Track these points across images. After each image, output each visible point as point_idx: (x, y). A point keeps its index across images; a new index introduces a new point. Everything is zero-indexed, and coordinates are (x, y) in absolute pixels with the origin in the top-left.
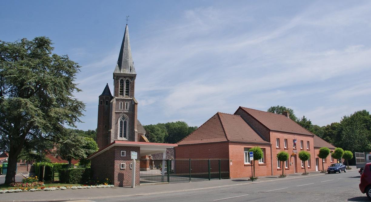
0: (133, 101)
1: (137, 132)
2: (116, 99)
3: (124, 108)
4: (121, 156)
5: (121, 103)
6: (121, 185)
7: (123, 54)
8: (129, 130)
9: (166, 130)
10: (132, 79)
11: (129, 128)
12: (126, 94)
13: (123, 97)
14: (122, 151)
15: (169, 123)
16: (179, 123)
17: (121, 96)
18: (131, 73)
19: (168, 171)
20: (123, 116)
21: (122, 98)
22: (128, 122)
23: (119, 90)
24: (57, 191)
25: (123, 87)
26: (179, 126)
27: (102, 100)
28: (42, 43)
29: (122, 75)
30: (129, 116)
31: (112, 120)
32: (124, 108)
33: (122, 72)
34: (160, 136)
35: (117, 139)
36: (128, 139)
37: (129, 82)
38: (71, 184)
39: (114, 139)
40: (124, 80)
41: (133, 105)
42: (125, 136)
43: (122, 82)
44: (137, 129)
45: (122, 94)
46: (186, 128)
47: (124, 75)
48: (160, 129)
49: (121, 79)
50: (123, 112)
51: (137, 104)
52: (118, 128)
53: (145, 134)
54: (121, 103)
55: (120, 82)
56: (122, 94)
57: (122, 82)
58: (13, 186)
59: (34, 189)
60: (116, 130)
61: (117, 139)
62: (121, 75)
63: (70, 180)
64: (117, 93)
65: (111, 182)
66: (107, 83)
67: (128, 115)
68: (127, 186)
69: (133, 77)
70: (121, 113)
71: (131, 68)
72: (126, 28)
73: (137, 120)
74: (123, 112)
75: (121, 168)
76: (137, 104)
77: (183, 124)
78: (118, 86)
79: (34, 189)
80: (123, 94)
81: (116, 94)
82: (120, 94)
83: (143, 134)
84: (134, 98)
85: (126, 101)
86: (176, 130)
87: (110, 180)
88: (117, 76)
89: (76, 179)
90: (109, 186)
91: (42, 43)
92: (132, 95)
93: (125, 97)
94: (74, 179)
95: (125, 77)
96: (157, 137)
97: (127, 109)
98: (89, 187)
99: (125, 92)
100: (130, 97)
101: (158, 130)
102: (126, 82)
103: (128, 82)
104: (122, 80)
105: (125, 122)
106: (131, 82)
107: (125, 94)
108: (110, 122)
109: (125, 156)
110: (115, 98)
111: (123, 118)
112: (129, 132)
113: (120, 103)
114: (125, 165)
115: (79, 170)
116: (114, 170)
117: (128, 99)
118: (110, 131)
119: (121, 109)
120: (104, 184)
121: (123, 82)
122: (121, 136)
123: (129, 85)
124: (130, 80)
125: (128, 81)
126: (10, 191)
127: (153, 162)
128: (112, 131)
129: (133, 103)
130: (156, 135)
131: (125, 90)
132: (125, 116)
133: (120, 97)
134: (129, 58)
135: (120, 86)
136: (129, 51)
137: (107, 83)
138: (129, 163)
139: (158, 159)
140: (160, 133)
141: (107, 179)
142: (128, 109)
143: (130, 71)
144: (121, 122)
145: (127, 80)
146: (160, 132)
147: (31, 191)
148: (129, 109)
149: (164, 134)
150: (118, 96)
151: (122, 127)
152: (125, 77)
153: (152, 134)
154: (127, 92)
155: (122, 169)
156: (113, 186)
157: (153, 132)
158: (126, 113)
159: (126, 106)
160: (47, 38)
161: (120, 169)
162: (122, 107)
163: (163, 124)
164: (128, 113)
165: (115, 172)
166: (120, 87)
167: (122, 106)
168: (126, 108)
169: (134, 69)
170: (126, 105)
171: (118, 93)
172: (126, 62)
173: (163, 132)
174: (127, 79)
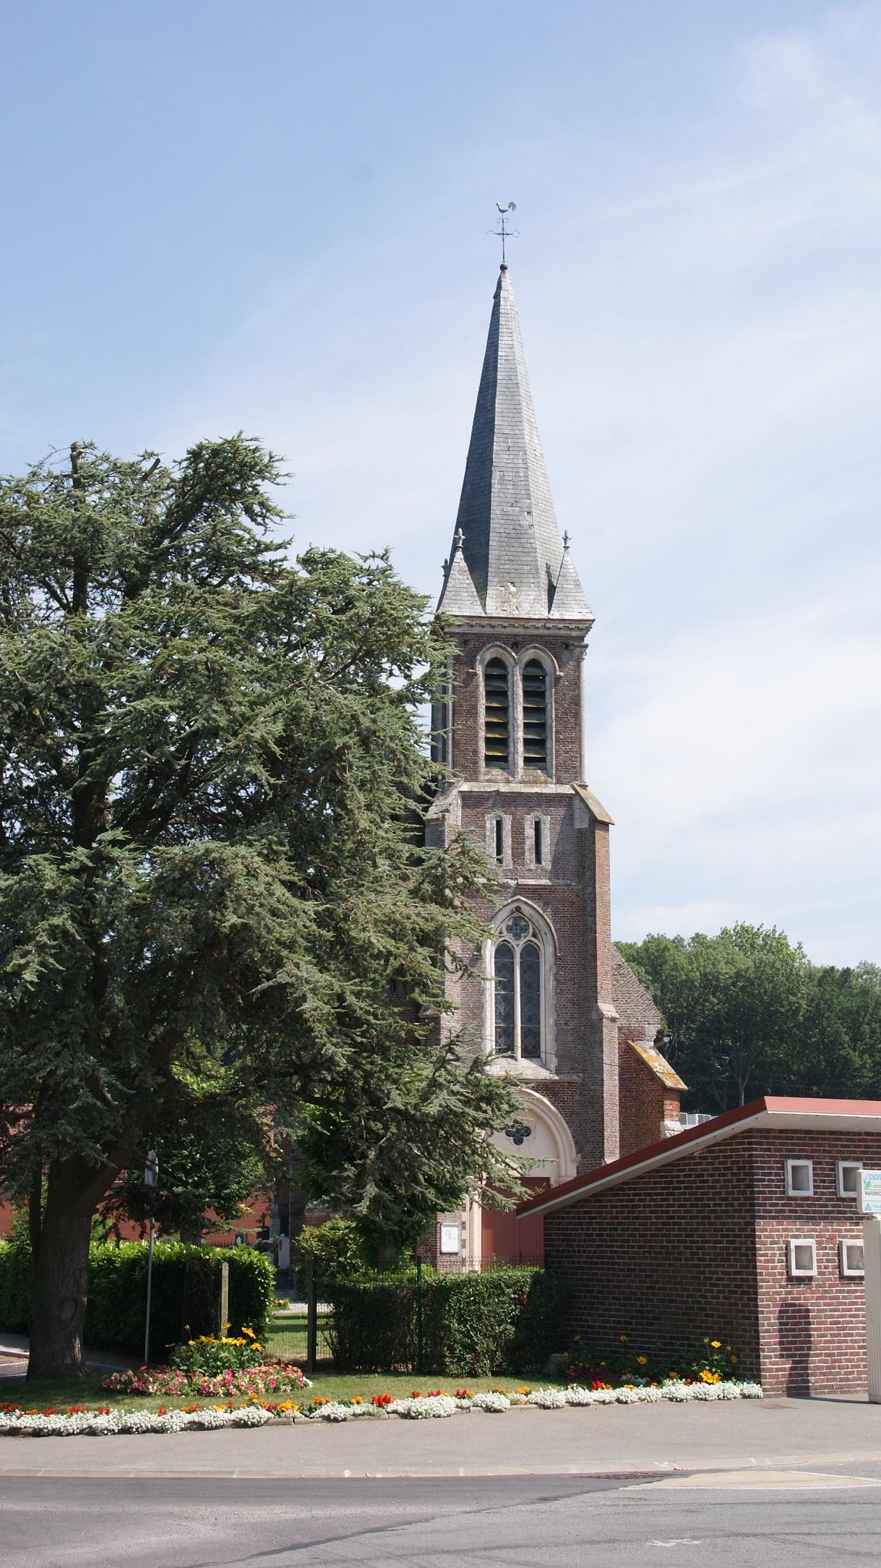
0: (577, 803)
1: (613, 1020)
2: (465, 796)
3: (518, 854)
4: (791, 1193)
5: (499, 824)
6: (798, 1388)
7: (495, 481)
8: (558, 1009)
10: (565, 654)
11: (559, 992)
12: (527, 760)
13: (508, 782)
14: (791, 1163)
16: (744, 938)
17: (496, 773)
18: (555, 615)
20: (518, 909)
21: (504, 788)
22: (550, 949)
23: (482, 734)
24: (466, 1417)
26: (745, 962)
28: (224, 476)
30: (555, 913)
32: (518, 854)
33: (494, 608)
36: (553, 1067)
38: (457, 1376)
40: (509, 662)
41: (583, 836)
42: (531, 1052)
43: (497, 672)
45: (500, 760)
46: (792, 976)
49: (489, 655)
50: (512, 883)
51: (605, 825)
53: (652, 1030)
54: (499, 824)
57: (497, 672)
58: (144, 1393)
59: (341, 1411)
62: (488, 630)
63: (452, 1349)
65: (741, 1366)
67: (546, 905)
68: (832, 1390)
69: (567, 642)
71: (549, 574)
72: (497, 296)
74: (512, 883)
75: (796, 1272)
76: (605, 825)
77: (775, 944)
78: (475, 707)
79: (341, 1411)
80: (504, 759)
82: (488, 758)
83: (640, 1035)
84: (584, 787)
85: (531, 810)
86: (715, 990)
87: (732, 1353)
89: (483, 1344)
90: (733, 1388)
91: (224, 476)
92: (572, 768)
93: (521, 780)
94: (470, 1348)
95: (516, 644)
97: (538, 860)
98: (583, 1394)
99: (521, 747)
100: (559, 782)
102: (526, 678)
104: (496, 663)
105: (531, 953)
106: (558, 679)
107: (521, 762)
109: (810, 1193)
110: (455, 792)
111: (518, 924)
112: (557, 1023)
113: (490, 824)
114: (814, 1252)
115: (496, 1287)
116: (756, 1287)
117: (545, 790)
120: (701, 1380)
121: (504, 678)
122: (505, 1047)
123: (542, 695)
124: (548, 661)
125: (533, 671)
126: (102, 1421)
131: (520, 734)
132: (525, 909)
133: (492, 781)
135: (482, 703)
136: (530, 456)
138: (832, 1238)
141: (716, 1344)
142: (547, 863)
143: (544, 597)
144: (503, 952)
145: (534, 663)
147: (327, 1419)
148: (555, 861)
151: (513, 990)
152: (516, 644)
154: (536, 744)
155: (800, 1280)
156: (753, 1388)
158: (534, 892)
159: (530, 843)
160: (253, 445)
161: (790, 1279)
164: (544, 887)
165: (762, 1301)
166: (488, 708)
168: (530, 855)
169: (578, 585)
170: (530, 832)
171: (476, 752)
172: (519, 535)
174: (529, 654)
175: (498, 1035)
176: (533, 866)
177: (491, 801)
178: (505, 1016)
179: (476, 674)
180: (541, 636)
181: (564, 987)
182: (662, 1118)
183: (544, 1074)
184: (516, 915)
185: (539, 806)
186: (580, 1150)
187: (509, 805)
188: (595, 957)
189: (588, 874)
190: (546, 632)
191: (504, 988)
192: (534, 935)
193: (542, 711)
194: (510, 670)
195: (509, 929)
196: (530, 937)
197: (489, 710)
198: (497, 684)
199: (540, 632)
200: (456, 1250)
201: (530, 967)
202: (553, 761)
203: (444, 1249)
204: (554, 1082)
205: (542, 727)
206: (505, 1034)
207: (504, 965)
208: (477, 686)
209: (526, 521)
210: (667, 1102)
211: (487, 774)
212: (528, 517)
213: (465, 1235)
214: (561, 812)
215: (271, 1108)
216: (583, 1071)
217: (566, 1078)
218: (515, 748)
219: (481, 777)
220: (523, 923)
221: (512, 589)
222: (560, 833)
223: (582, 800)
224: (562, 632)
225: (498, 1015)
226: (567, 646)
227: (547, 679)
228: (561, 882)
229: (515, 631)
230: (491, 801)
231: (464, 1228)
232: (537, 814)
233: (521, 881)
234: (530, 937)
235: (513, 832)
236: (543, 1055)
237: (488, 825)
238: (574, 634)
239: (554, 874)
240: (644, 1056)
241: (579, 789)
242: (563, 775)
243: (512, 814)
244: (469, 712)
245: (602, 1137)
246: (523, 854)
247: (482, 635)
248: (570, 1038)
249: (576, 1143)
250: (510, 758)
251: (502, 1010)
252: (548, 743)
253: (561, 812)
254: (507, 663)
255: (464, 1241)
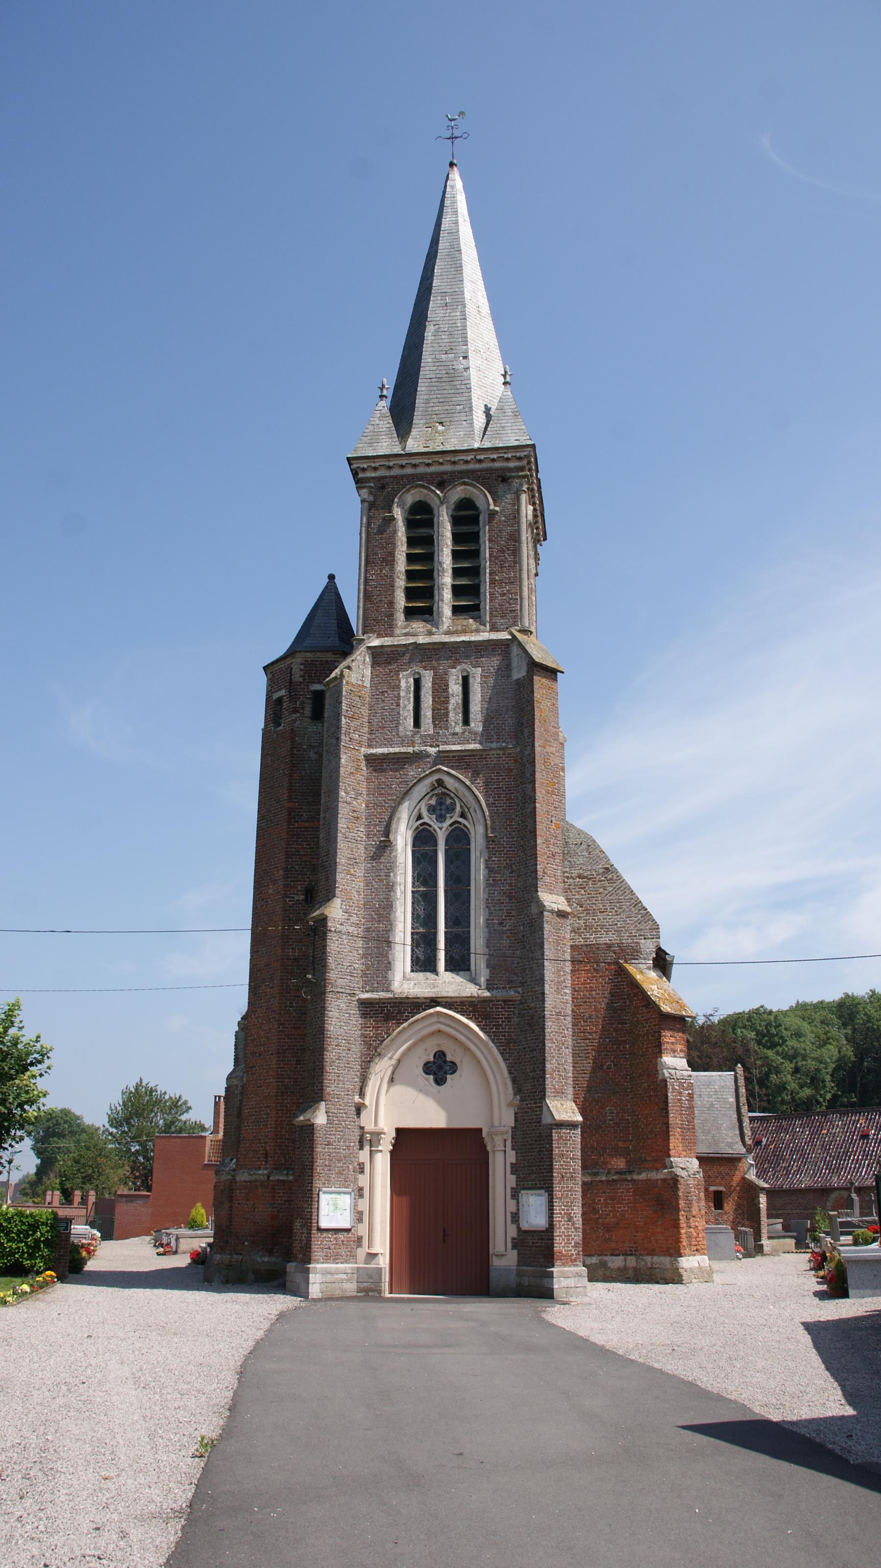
0: (515, 650)
1: (562, 914)
3: (441, 716)
5: (418, 683)
9: (839, 1034)
10: (502, 487)
11: (492, 883)
12: (456, 610)
13: (430, 633)
15: (853, 998)
17: (418, 626)
19: (307, 897)
21: (422, 640)
22: (481, 830)
25: (429, 557)
27: (283, 693)
29: (422, 470)
30: (487, 784)
31: (342, 824)
32: (441, 716)
33: (414, 444)
34: (812, 1064)
35: (388, 990)
36: (483, 980)
37: (475, 520)
39: (357, 983)
40: (434, 502)
42: (458, 963)
43: (421, 519)
44: (566, 892)
47: (433, 469)
48: (806, 1027)
49: (410, 498)
50: (432, 751)
52: (390, 887)
54: (418, 683)
55: (410, 524)
56: (421, 605)
57: (421, 519)
60: (380, 912)
61: (388, 990)
62: (409, 471)
64: (384, 608)
66: (332, 577)
67: (476, 774)
70: (417, 757)
73: (567, 828)
76: (552, 673)
78: (392, 554)
81: (378, 617)
84: (526, 632)
88: (381, 484)
92: (510, 612)
93: (447, 627)
96: (796, 1070)
97: (466, 721)
99: (447, 595)
100: (494, 628)
101: (798, 1035)
102: (456, 521)
103: (466, 518)
105: (459, 840)
106: (492, 514)
107: (447, 611)
108: (322, 842)
110: (363, 648)
111: (442, 803)
112: (488, 923)
113: (406, 683)
118: (323, 920)
119: (417, 723)
121: (429, 523)
122: (424, 963)
124: (486, 501)
127: (763, 1200)
128: (340, 914)
129: (519, 673)
130: (791, 1058)
132: (449, 782)
134: (471, 355)
137: (332, 577)
139: (805, 1182)
140: (809, 1047)
142: (477, 725)
144: (423, 840)
146: (807, 1044)
149: (831, 1052)
150: (388, 629)
151: (435, 885)
153: (770, 1053)
154: (468, 601)
157: (773, 1045)
158: (460, 760)
162: (427, 713)
163: (820, 1006)
167: (427, 701)
168: (455, 717)
170: (455, 688)
171: (391, 603)
173: (823, 1043)
174: (458, 493)
175: (415, 944)
176: (458, 729)
177: (407, 656)
178: (424, 918)
179: (393, 519)
180: (472, 472)
181: (498, 877)
182: (660, 1053)
183: (470, 990)
184: (439, 790)
185: (468, 657)
186: (518, 1090)
187: (430, 659)
188: (534, 833)
189: (526, 731)
190: (478, 466)
191: (425, 883)
192: (463, 815)
193: (475, 554)
194: (436, 512)
195: (431, 809)
196: (456, 817)
197: (410, 558)
198: (422, 531)
199: (471, 466)
200: (347, 1225)
201: (458, 855)
202: (487, 606)
203: (324, 1223)
204: (484, 1001)
205: (475, 572)
206: (424, 942)
207: (425, 855)
208: (395, 532)
209: (461, 364)
210: (668, 1033)
211: (406, 627)
212: (464, 362)
213: (363, 1205)
214: (494, 662)
215: (781, 1220)
216: (522, 984)
217: (500, 994)
218: (441, 595)
219: (398, 631)
220: (449, 801)
221: (440, 428)
222: (494, 687)
223: (520, 645)
224: (497, 465)
225: (415, 917)
226: (504, 480)
227: (481, 518)
228: (494, 745)
229: (441, 468)
230: (407, 656)
231: (361, 1196)
232: (465, 666)
233: (442, 748)
234: (456, 817)
235: (434, 690)
236: (473, 968)
237: (403, 684)
238: (512, 465)
239: (487, 736)
240: (638, 977)
241: (519, 636)
242: (499, 621)
243: (434, 669)
244: (384, 560)
245: (543, 1070)
246: (447, 715)
247: (402, 477)
248: (506, 943)
249: (514, 1081)
250: (435, 609)
251: (421, 913)
252: (482, 587)
253: (494, 662)
254: (433, 505)
255: (361, 1213)
